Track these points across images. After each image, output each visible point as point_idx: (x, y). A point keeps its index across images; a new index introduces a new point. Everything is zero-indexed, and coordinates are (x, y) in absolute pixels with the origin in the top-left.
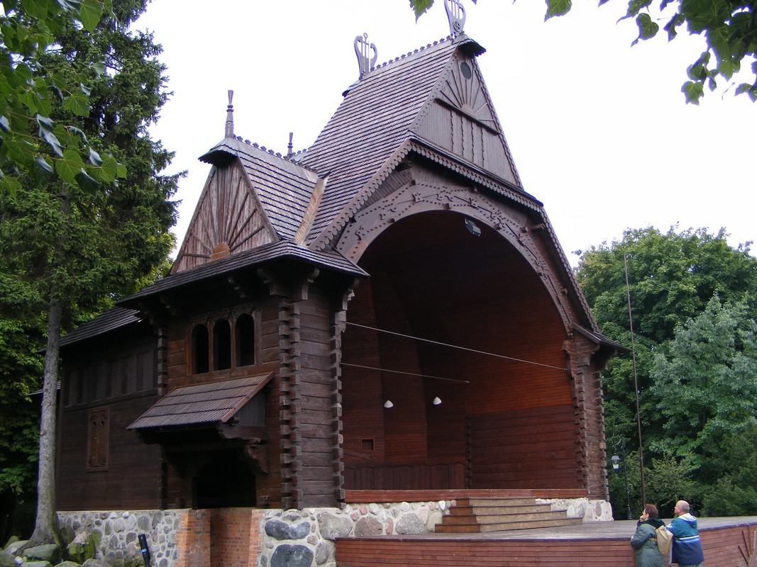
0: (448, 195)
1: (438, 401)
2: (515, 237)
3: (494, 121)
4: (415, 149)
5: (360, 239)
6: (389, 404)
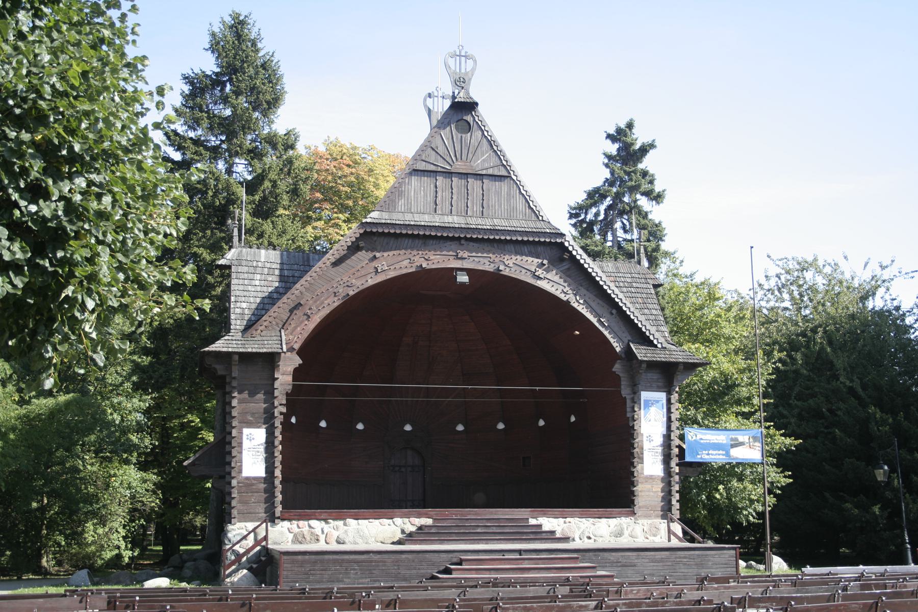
2: (529, 273)
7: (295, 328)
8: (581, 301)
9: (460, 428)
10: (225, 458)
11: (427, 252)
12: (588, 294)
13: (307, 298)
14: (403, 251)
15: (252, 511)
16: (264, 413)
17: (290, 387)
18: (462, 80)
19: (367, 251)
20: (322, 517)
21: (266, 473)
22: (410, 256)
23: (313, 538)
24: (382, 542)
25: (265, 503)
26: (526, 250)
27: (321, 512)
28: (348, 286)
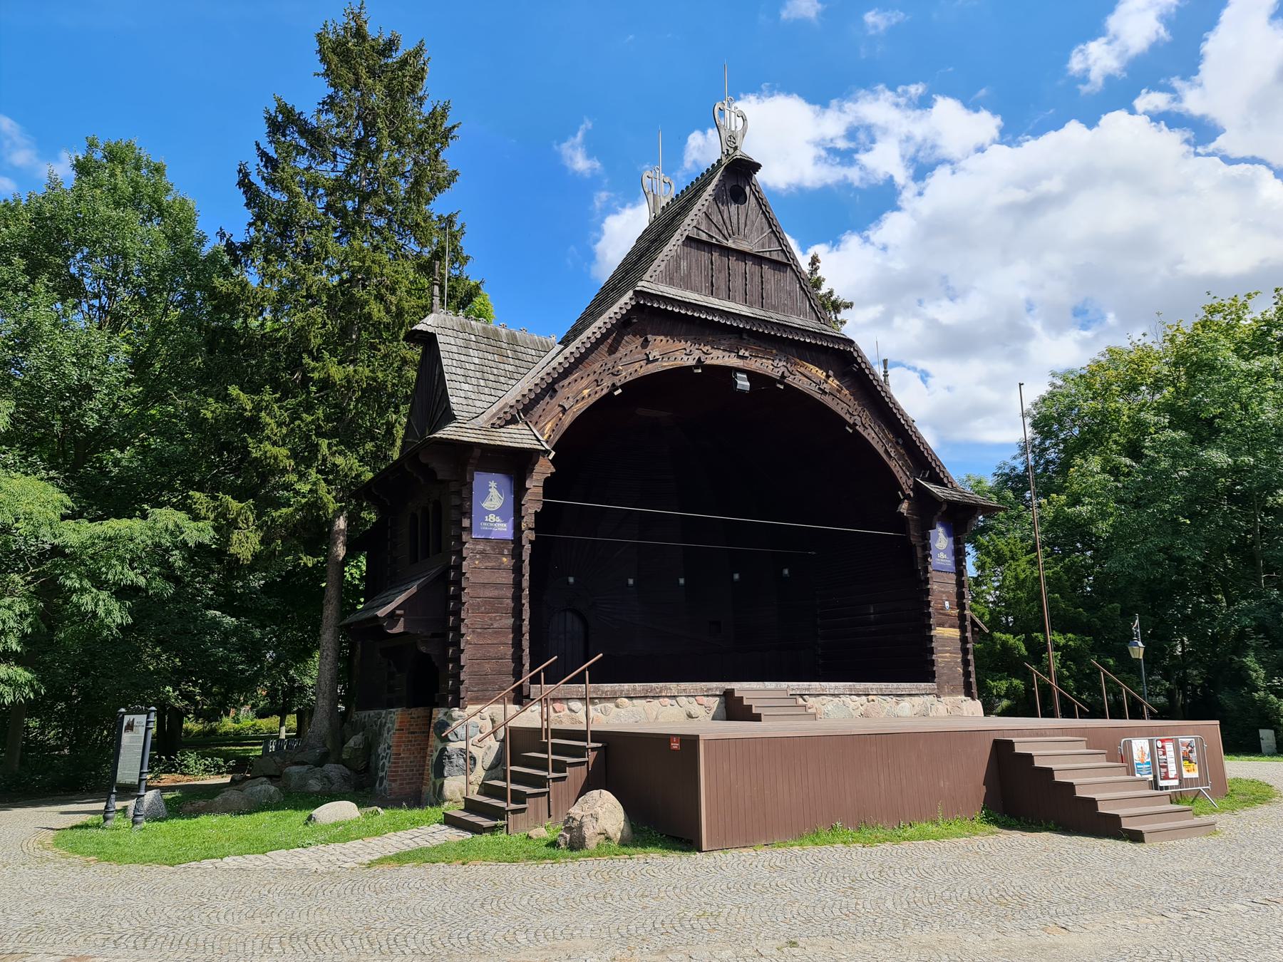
1: (736, 576)
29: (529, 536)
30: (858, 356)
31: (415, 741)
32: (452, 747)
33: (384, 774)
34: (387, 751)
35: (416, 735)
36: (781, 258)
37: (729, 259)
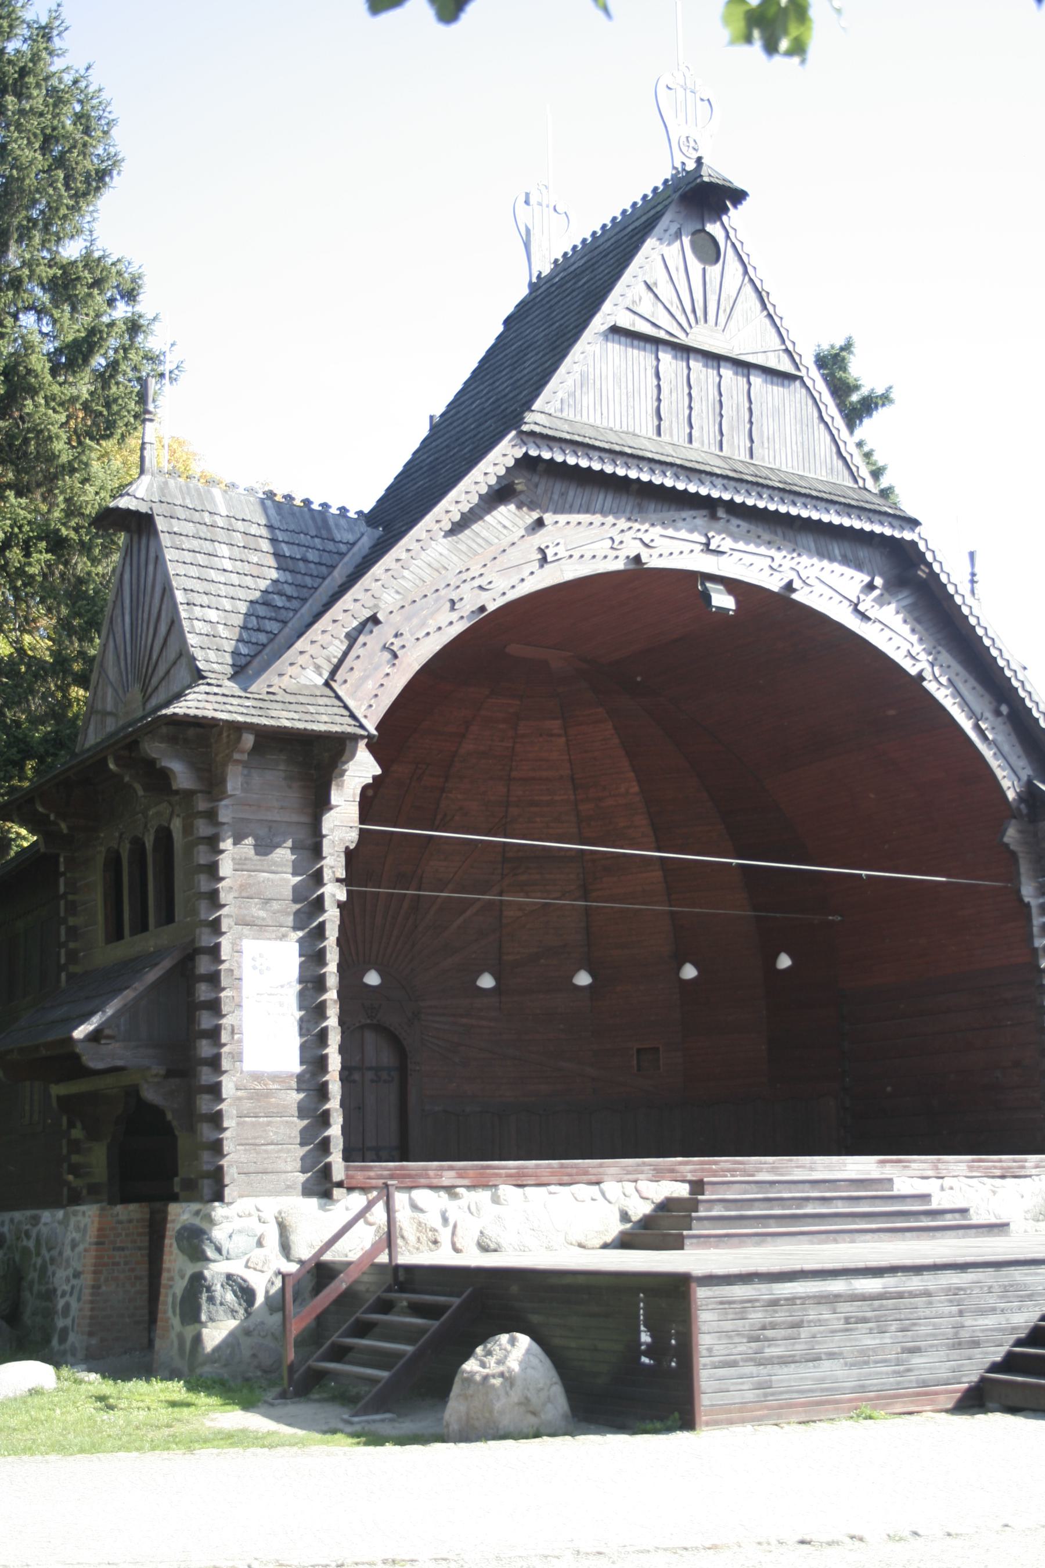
0: (639, 535)
1: (784, 962)
2: (846, 603)
3: (787, 351)
4: (533, 453)
5: (395, 656)
6: (689, 972)
7: (364, 679)
8: (944, 680)
9: (487, 981)
10: (192, 1020)
11: (646, 526)
12: (956, 667)
13: (388, 600)
14: (597, 519)
15: (270, 1167)
16: (295, 900)
17: (354, 835)
18: (692, 144)
19: (519, 507)
20: (445, 1182)
21: (302, 1063)
22: (614, 532)
23: (424, 1239)
24: (581, 1246)
25: (302, 1144)
26: (837, 552)
27: (442, 1169)
28: (480, 587)
29: (334, 893)
30: (928, 549)
31: (126, 1263)
32: (216, 1270)
33: (68, 1322)
34: (74, 1282)
35: (127, 1252)
36: (786, 366)
37: (689, 368)
